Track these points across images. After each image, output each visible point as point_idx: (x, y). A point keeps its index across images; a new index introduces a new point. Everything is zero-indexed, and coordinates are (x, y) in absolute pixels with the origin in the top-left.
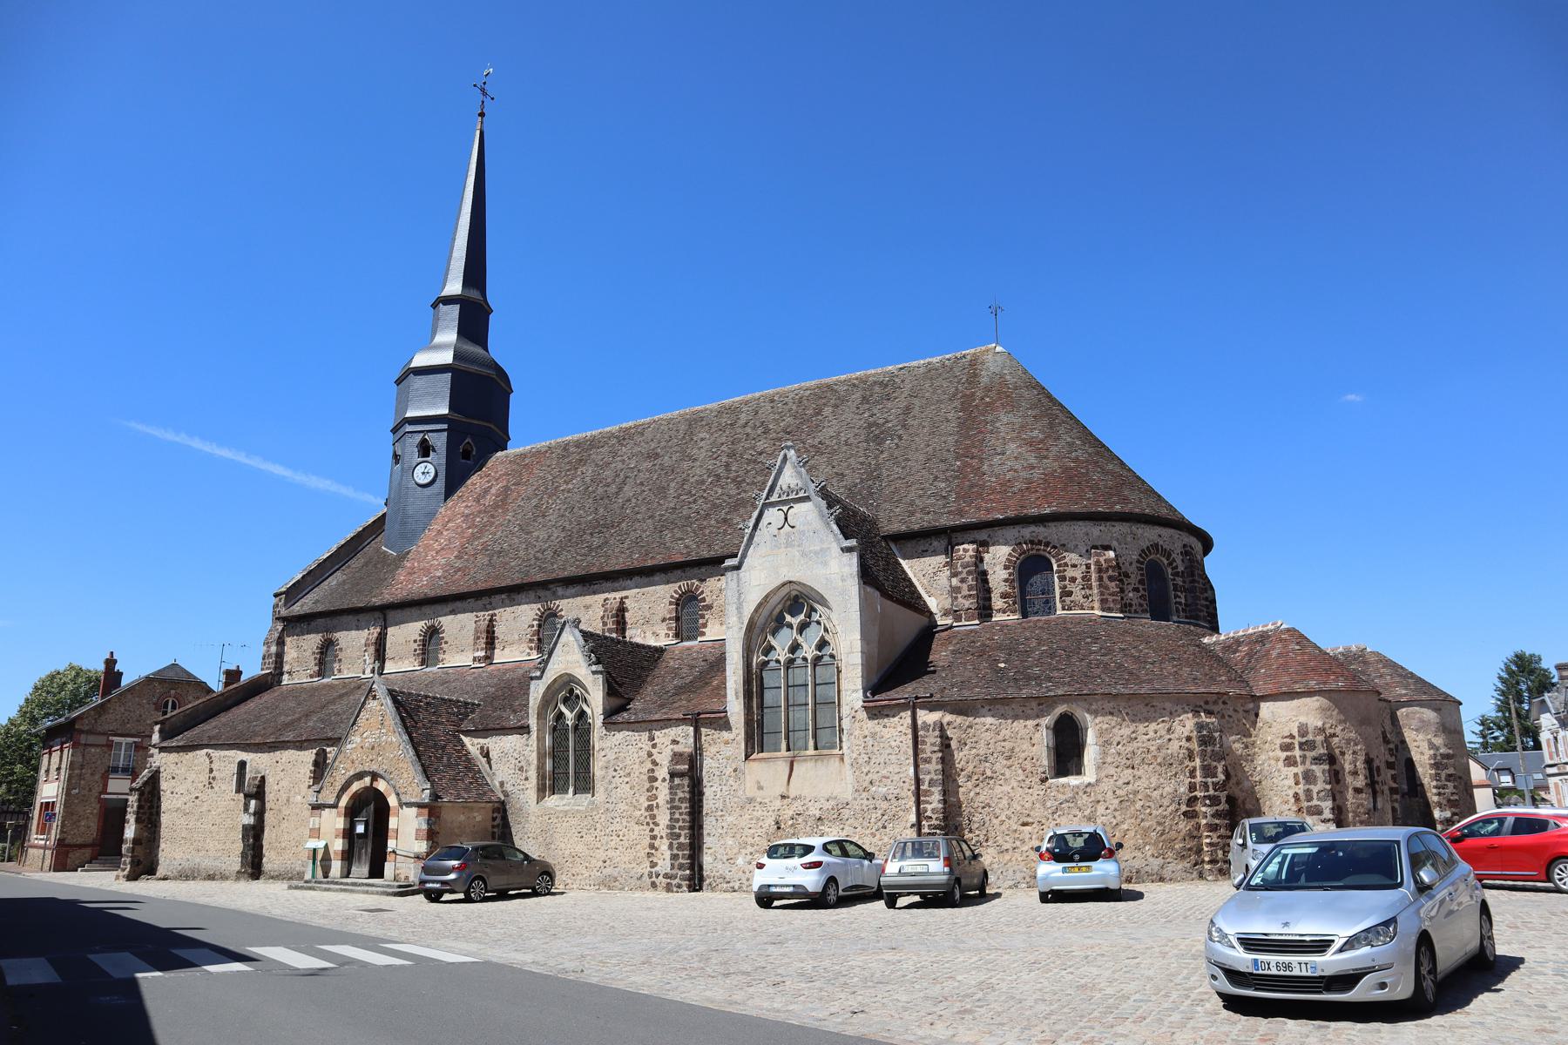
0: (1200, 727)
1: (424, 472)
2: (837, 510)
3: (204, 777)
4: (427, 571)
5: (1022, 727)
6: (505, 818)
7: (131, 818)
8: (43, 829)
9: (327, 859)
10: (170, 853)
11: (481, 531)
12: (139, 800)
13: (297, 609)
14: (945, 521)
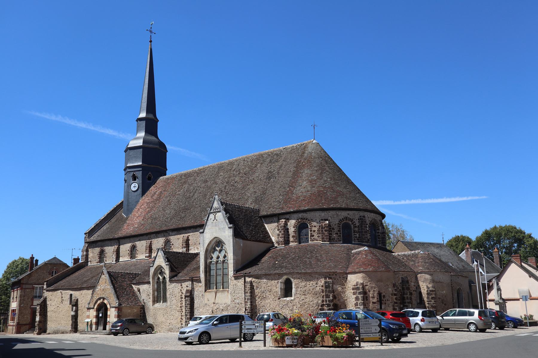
0: (326, 282)
1: (134, 186)
2: (228, 215)
3: (60, 300)
4: (133, 225)
5: (274, 282)
6: (144, 311)
7: (38, 314)
8: (13, 319)
9: (91, 325)
10: (51, 326)
11: (151, 210)
12: (40, 308)
13: (93, 239)
14: (278, 211)
